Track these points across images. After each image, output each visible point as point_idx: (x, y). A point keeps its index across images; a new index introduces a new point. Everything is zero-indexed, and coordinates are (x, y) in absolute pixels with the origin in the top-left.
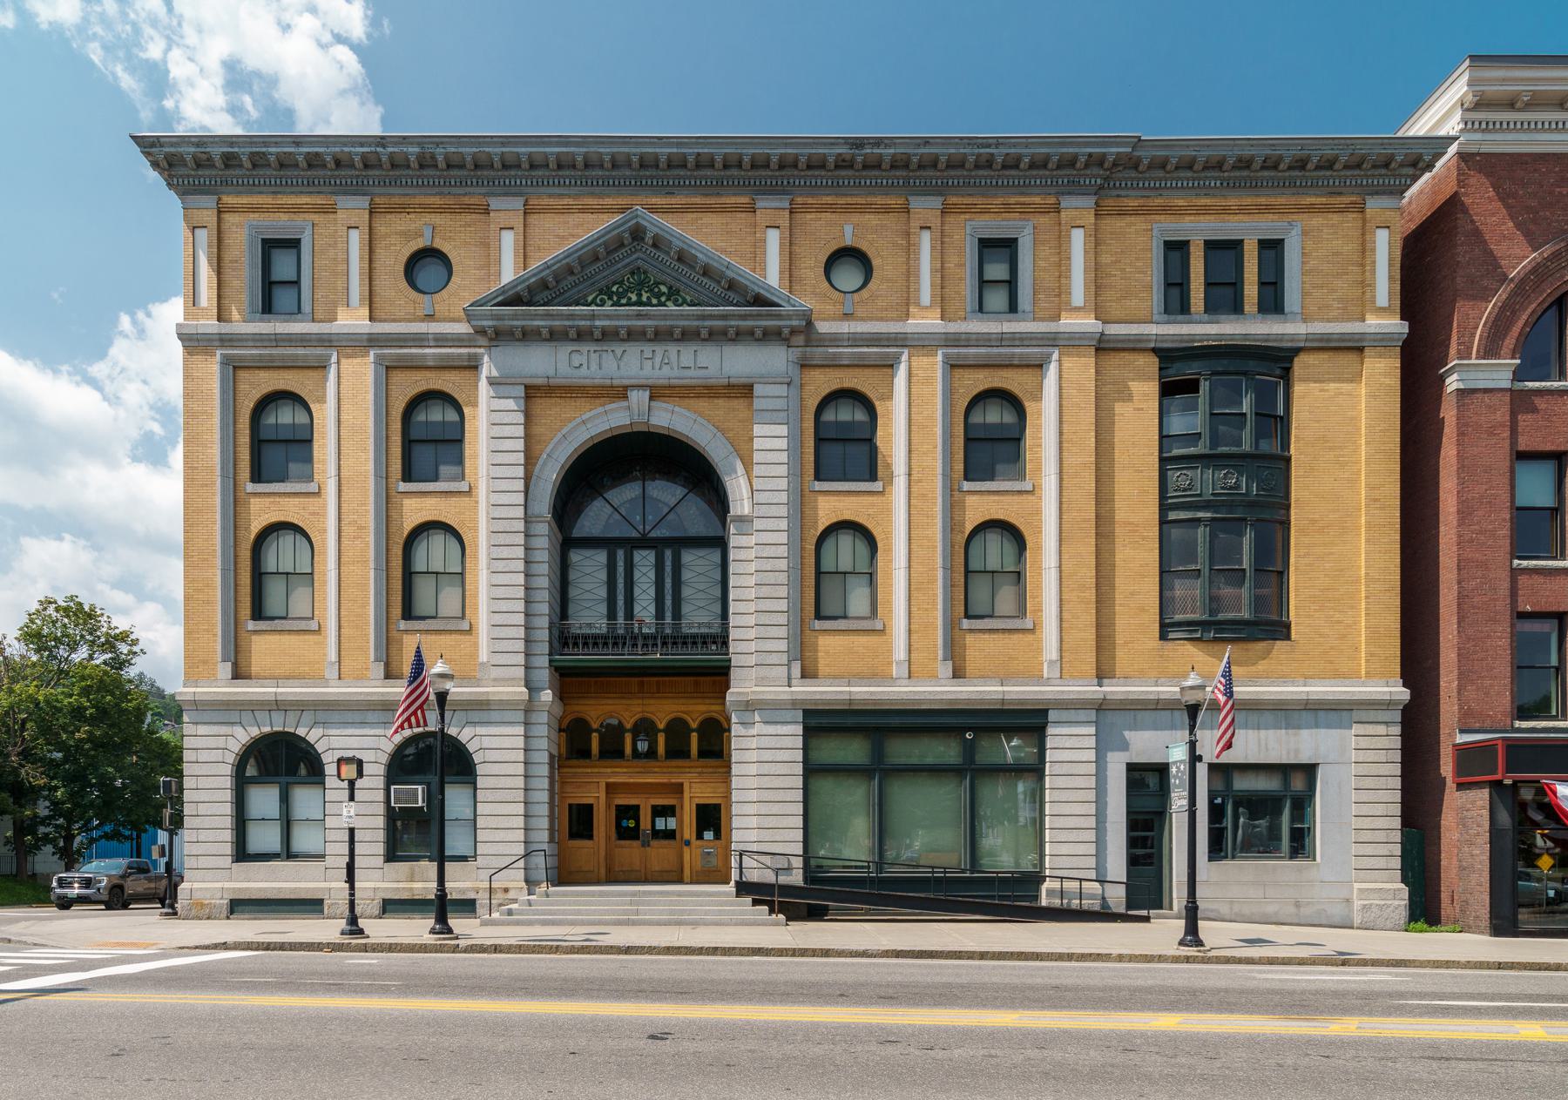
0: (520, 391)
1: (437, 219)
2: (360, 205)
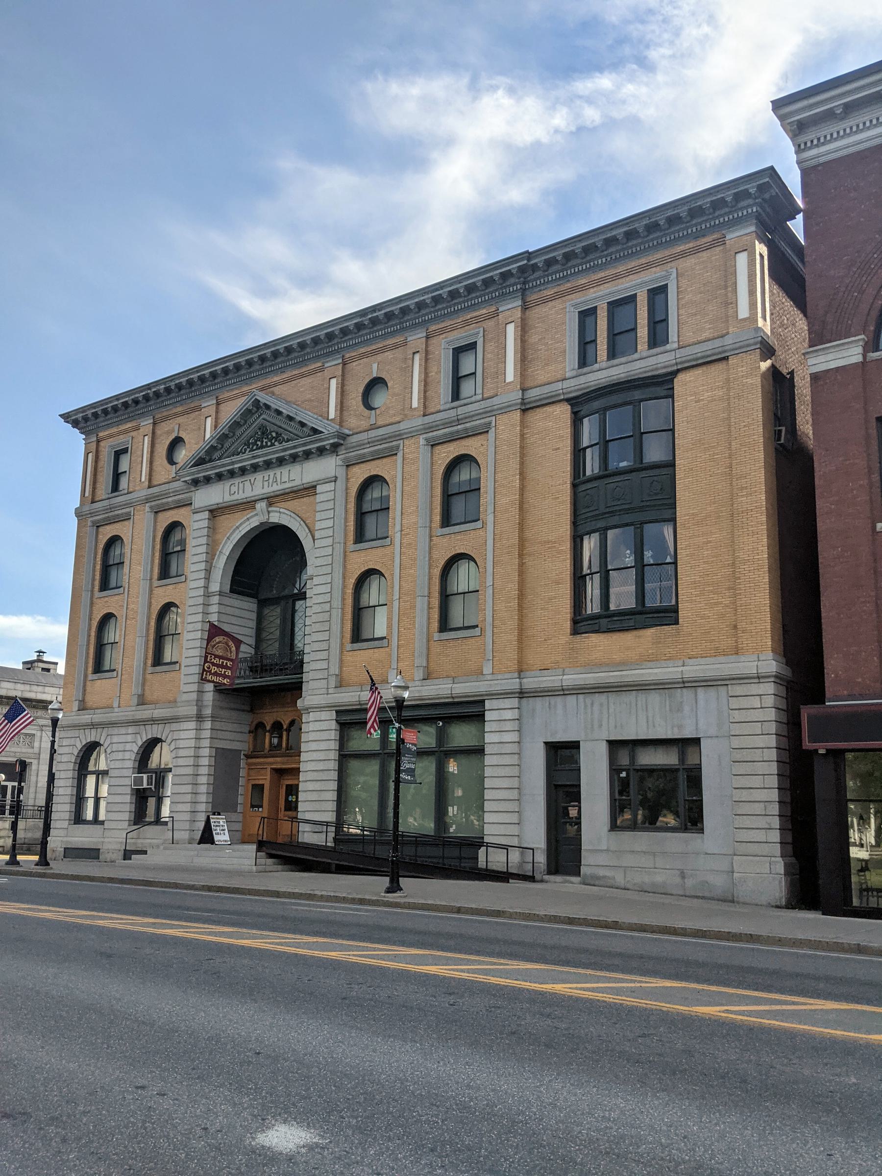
0: (206, 515)
1: (180, 420)
2: (515, 304)
